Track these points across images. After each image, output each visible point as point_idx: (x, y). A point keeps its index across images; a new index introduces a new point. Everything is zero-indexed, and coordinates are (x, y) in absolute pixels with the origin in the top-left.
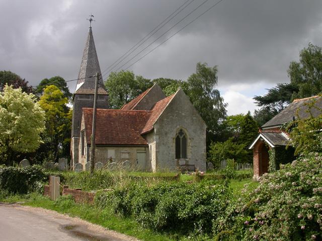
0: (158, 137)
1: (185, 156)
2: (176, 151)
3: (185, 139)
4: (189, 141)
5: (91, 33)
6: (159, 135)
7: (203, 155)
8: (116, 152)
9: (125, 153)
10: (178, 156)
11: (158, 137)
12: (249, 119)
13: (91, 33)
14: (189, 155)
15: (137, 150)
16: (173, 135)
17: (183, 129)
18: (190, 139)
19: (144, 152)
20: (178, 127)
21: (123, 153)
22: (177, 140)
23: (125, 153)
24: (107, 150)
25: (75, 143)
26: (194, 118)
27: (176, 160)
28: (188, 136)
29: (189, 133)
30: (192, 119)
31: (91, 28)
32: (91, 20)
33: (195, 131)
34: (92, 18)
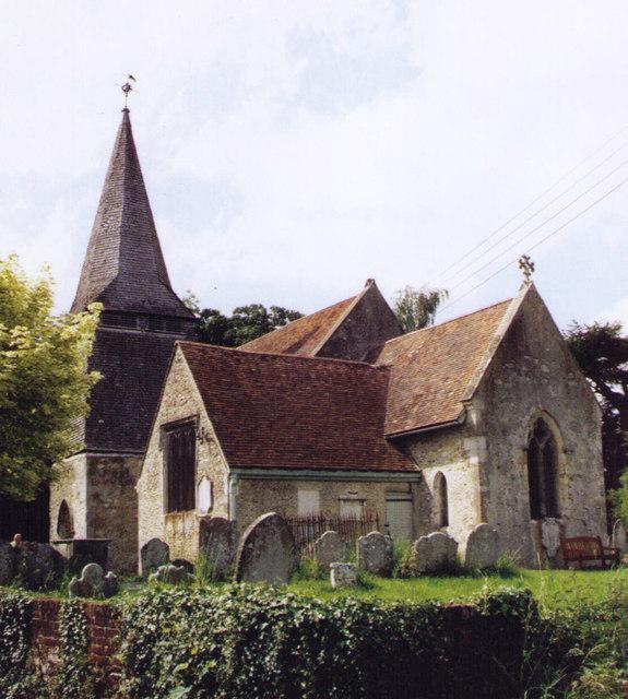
0: (482, 441)
1: (554, 511)
2: (531, 494)
3: (550, 453)
4: (562, 457)
5: (127, 127)
6: (485, 434)
7: (598, 503)
8: (324, 496)
9: (354, 500)
10: (536, 513)
11: (482, 441)
12: (107, 477)
13: (127, 127)
14: (565, 505)
15: (388, 491)
16: (520, 438)
17: (545, 417)
18: (565, 452)
19: (408, 497)
20: (533, 409)
21: (345, 500)
22: (531, 452)
23: (354, 500)
24: (295, 490)
25: (142, 556)
26: (572, 383)
27: (534, 522)
28: (560, 444)
29: (561, 435)
30: (567, 386)
31: (126, 111)
32: (128, 89)
33: (575, 427)
34: (131, 82)
